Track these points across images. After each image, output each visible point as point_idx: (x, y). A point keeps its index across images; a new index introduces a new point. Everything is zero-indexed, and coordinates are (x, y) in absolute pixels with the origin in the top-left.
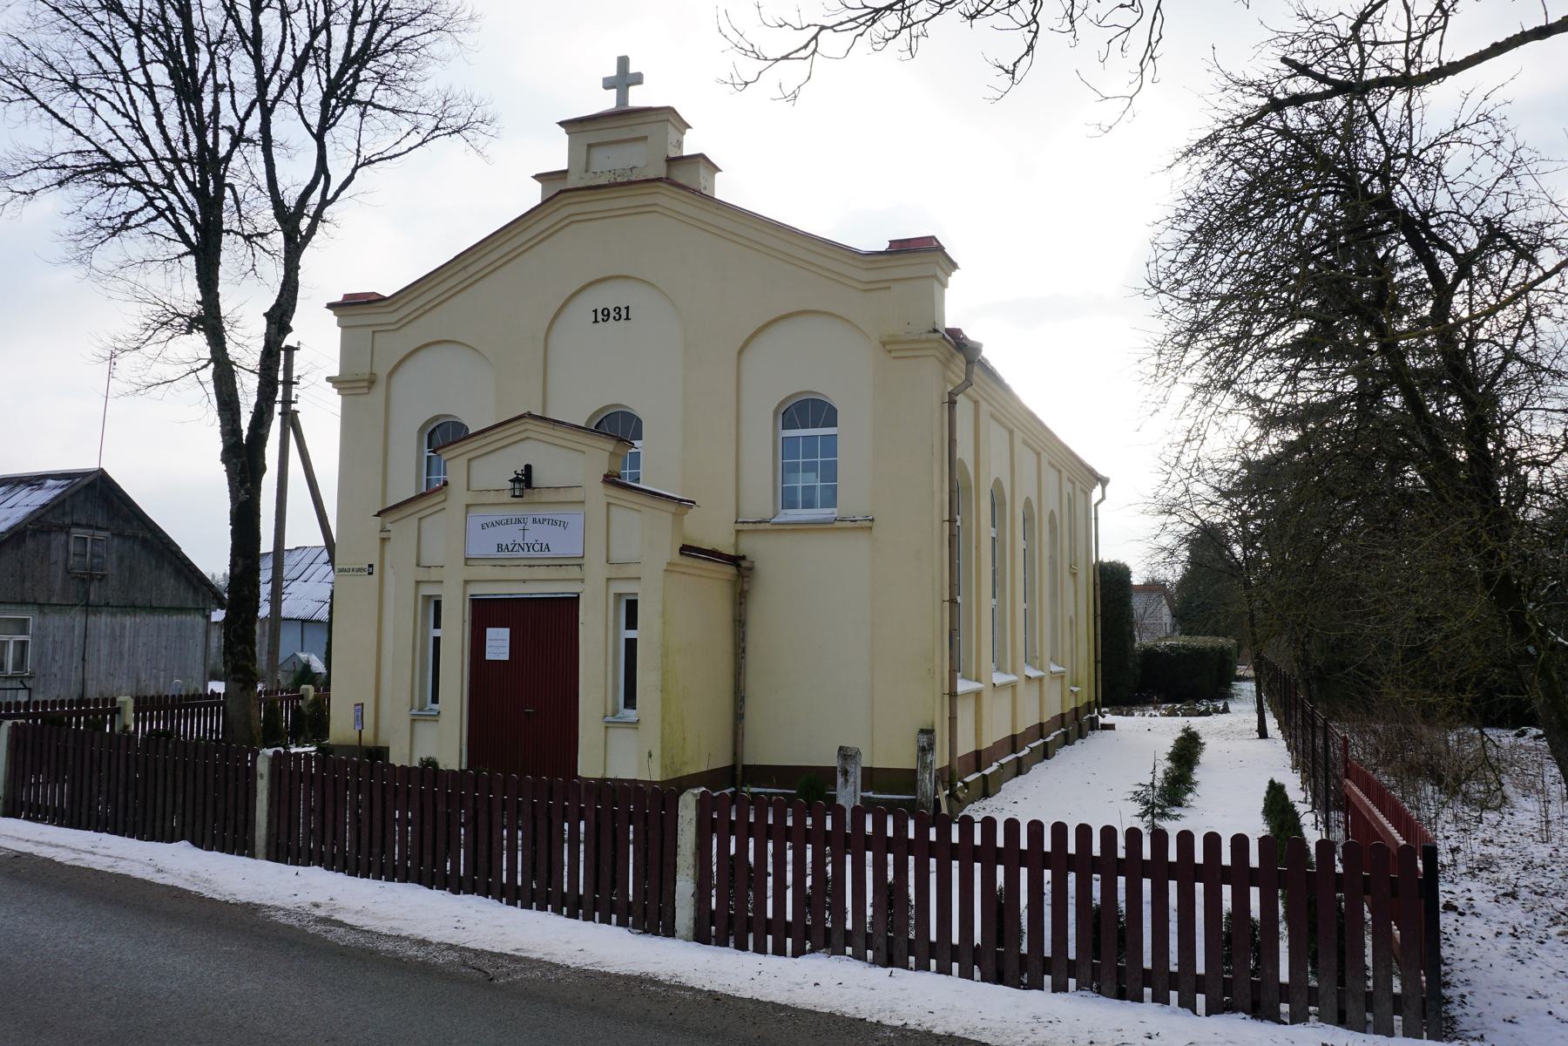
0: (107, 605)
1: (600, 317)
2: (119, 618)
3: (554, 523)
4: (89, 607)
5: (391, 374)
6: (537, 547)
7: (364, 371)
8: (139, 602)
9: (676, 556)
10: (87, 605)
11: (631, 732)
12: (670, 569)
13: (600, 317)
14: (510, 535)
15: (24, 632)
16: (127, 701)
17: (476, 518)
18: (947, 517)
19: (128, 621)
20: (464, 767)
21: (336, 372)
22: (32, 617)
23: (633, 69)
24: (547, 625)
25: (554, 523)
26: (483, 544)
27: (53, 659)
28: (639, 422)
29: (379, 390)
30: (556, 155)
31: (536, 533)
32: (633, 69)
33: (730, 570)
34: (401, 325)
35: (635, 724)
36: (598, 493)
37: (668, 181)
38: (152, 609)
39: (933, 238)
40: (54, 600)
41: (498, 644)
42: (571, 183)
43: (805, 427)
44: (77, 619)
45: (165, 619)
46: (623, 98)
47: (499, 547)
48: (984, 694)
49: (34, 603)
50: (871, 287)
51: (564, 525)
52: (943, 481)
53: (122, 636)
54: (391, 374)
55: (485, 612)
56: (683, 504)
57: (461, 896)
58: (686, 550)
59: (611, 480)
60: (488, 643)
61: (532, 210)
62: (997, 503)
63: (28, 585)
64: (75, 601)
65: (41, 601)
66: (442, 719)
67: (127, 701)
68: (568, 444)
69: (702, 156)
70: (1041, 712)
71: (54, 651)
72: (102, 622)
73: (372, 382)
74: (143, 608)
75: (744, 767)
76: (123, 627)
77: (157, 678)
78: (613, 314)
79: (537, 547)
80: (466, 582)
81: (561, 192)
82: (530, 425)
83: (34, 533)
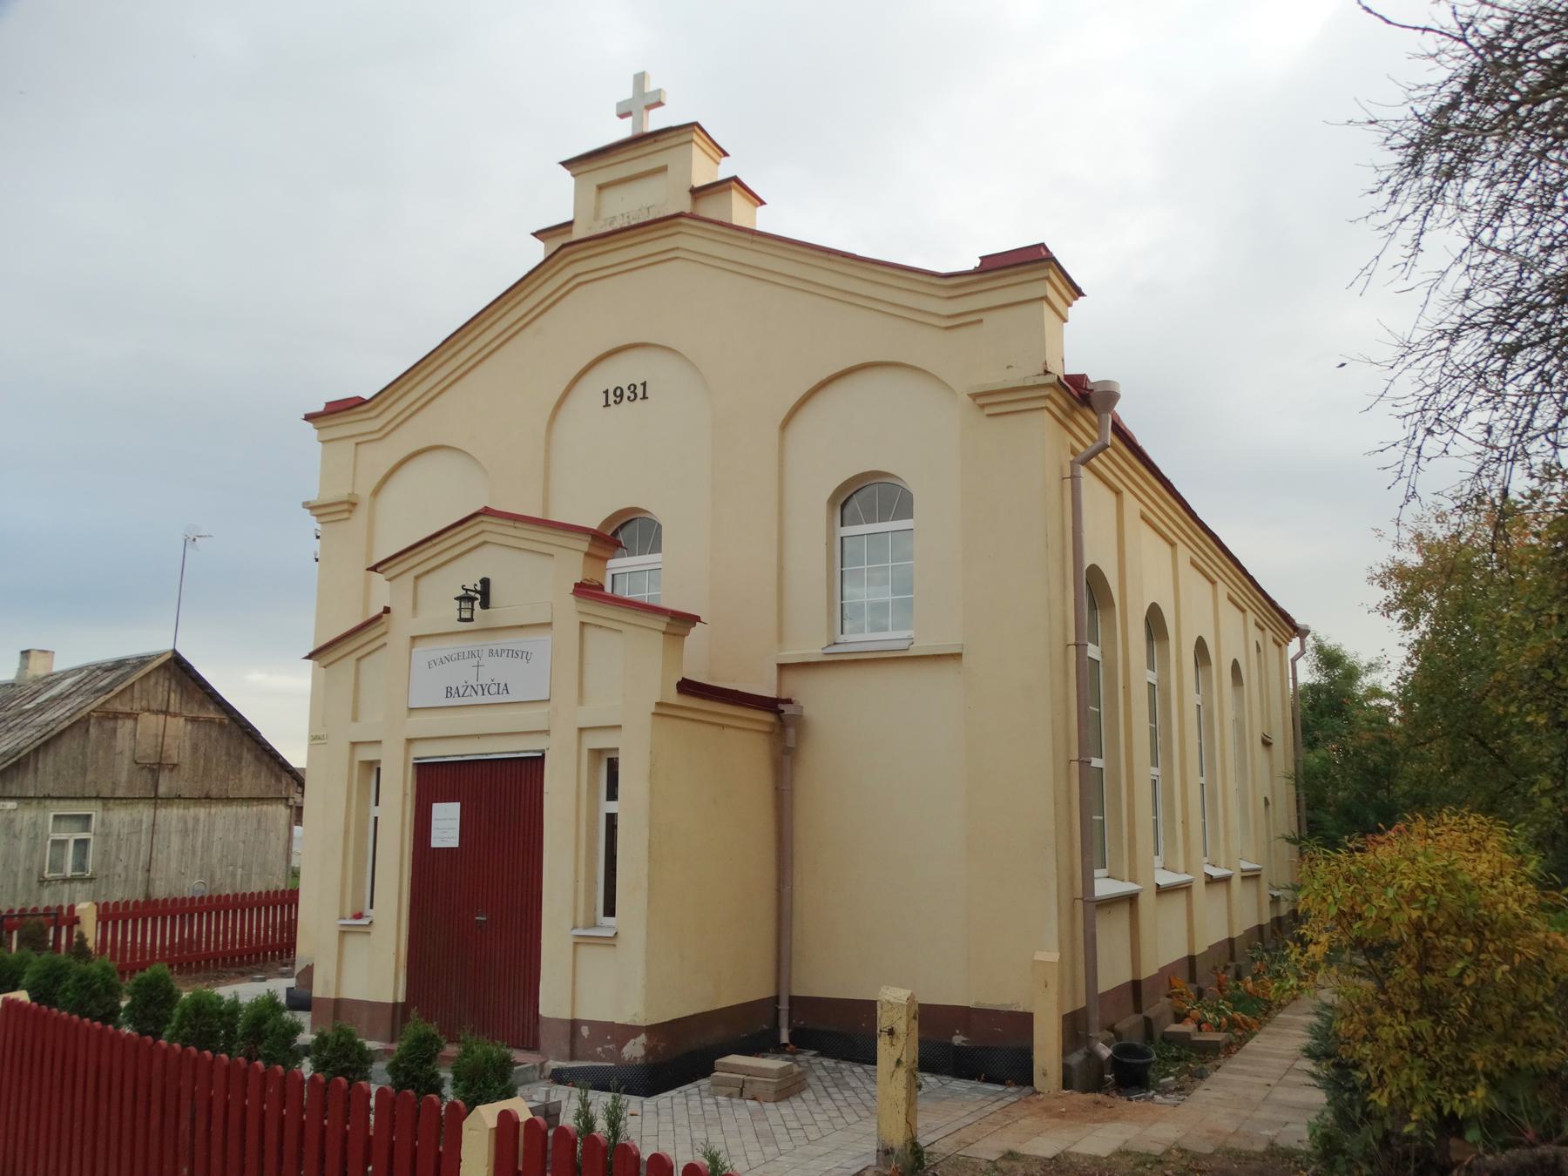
0: (179, 797)
1: (612, 398)
2: (192, 811)
3: (515, 654)
4: (156, 799)
5: (376, 492)
6: (494, 689)
7: (341, 493)
8: (214, 793)
9: (674, 697)
10: (156, 797)
11: (603, 950)
12: (663, 710)
13: (612, 398)
14: (462, 673)
15: (87, 829)
16: (86, 910)
17: (423, 652)
18: (1072, 640)
19: (202, 812)
20: (401, 999)
21: (313, 496)
22: (94, 810)
23: (651, 87)
24: (500, 795)
25: (515, 654)
26: (427, 689)
27: (117, 858)
28: (660, 526)
29: (361, 514)
30: (559, 200)
31: (494, 669)
32: (651, 87)
33: (769, 717)
34: (384, 434)
35: (611, 941)
36: (569, 609)
37: (692, 216)
38: (228, 800)
39: (1043, 245)
40: (119, 794)
41: (447, 825)
42: (578, 233)
43: (870, 520)
44: (144, 813)
45: (242, 810)
46: (639, 122)
47: (449, 691)
48: (1142, 899)
49: (97, 798)
50: (957, 322)
51: (525, 655)
52: (1065, 587)
53: (195, 830)
54: (376, 492)
55: (434, 780)
56: (683, 621)
57: (463, 1156)
58: (687, 687)
59: (587, 590)
60: (434, 824)
61: (530, 273)
62: (1154, 620)
63: (90, 777)
64: (142, 793)
65: (106, 793)
66: (374, 931)
67: (86, 910)
68: (535, 546)
69: (696, 124)
70: (1230, 921)
71: (119, 848)
72: (172, 815)
73: (353, 505)
74: (219, 799)
75: (793, 1000)
76: (197, 820)
77: (234, 875)
78: (627, 393)
79: (494, 689)
80: (410, 741)
81: (564, 246)
82: (487, 524)
83: (100, 720)
